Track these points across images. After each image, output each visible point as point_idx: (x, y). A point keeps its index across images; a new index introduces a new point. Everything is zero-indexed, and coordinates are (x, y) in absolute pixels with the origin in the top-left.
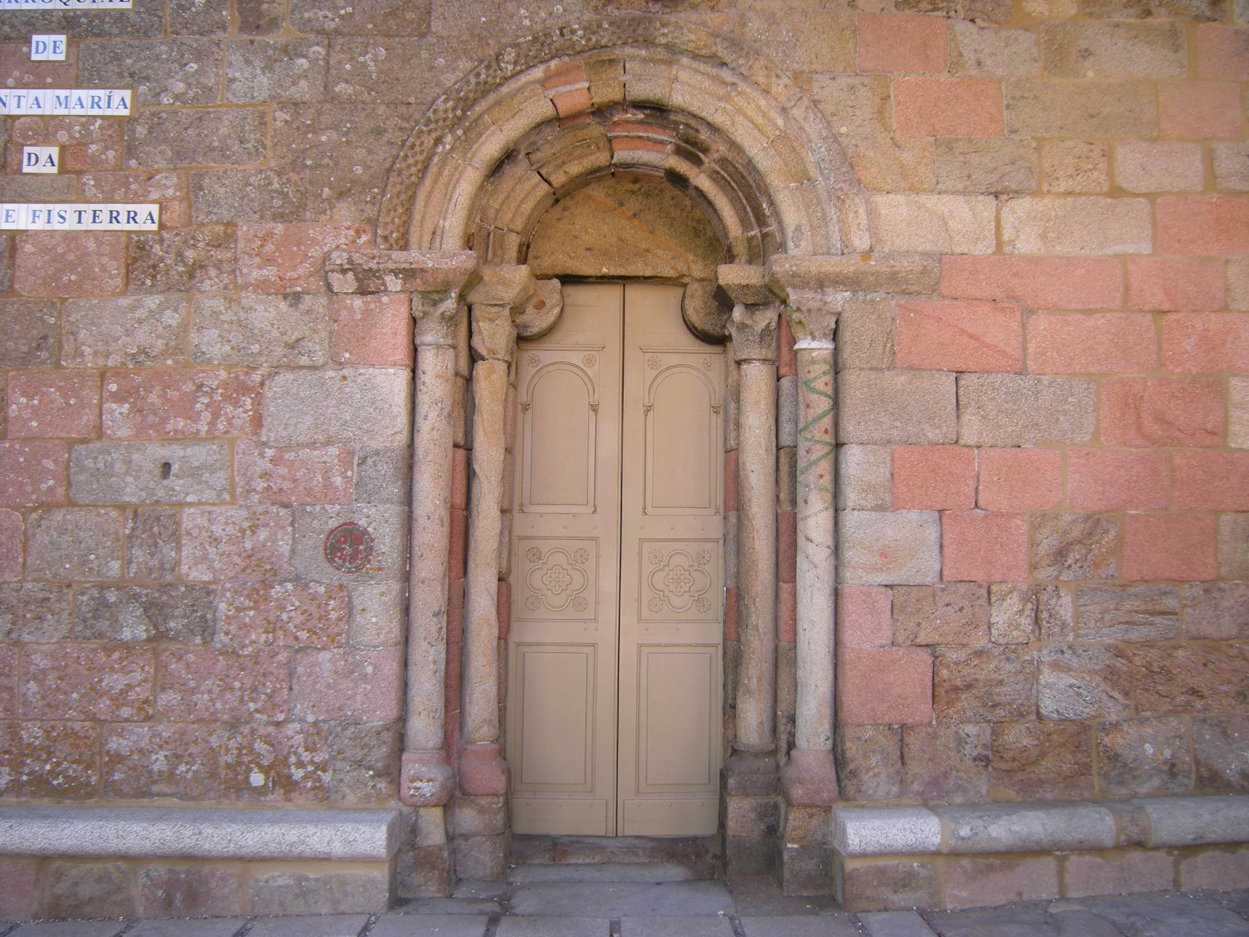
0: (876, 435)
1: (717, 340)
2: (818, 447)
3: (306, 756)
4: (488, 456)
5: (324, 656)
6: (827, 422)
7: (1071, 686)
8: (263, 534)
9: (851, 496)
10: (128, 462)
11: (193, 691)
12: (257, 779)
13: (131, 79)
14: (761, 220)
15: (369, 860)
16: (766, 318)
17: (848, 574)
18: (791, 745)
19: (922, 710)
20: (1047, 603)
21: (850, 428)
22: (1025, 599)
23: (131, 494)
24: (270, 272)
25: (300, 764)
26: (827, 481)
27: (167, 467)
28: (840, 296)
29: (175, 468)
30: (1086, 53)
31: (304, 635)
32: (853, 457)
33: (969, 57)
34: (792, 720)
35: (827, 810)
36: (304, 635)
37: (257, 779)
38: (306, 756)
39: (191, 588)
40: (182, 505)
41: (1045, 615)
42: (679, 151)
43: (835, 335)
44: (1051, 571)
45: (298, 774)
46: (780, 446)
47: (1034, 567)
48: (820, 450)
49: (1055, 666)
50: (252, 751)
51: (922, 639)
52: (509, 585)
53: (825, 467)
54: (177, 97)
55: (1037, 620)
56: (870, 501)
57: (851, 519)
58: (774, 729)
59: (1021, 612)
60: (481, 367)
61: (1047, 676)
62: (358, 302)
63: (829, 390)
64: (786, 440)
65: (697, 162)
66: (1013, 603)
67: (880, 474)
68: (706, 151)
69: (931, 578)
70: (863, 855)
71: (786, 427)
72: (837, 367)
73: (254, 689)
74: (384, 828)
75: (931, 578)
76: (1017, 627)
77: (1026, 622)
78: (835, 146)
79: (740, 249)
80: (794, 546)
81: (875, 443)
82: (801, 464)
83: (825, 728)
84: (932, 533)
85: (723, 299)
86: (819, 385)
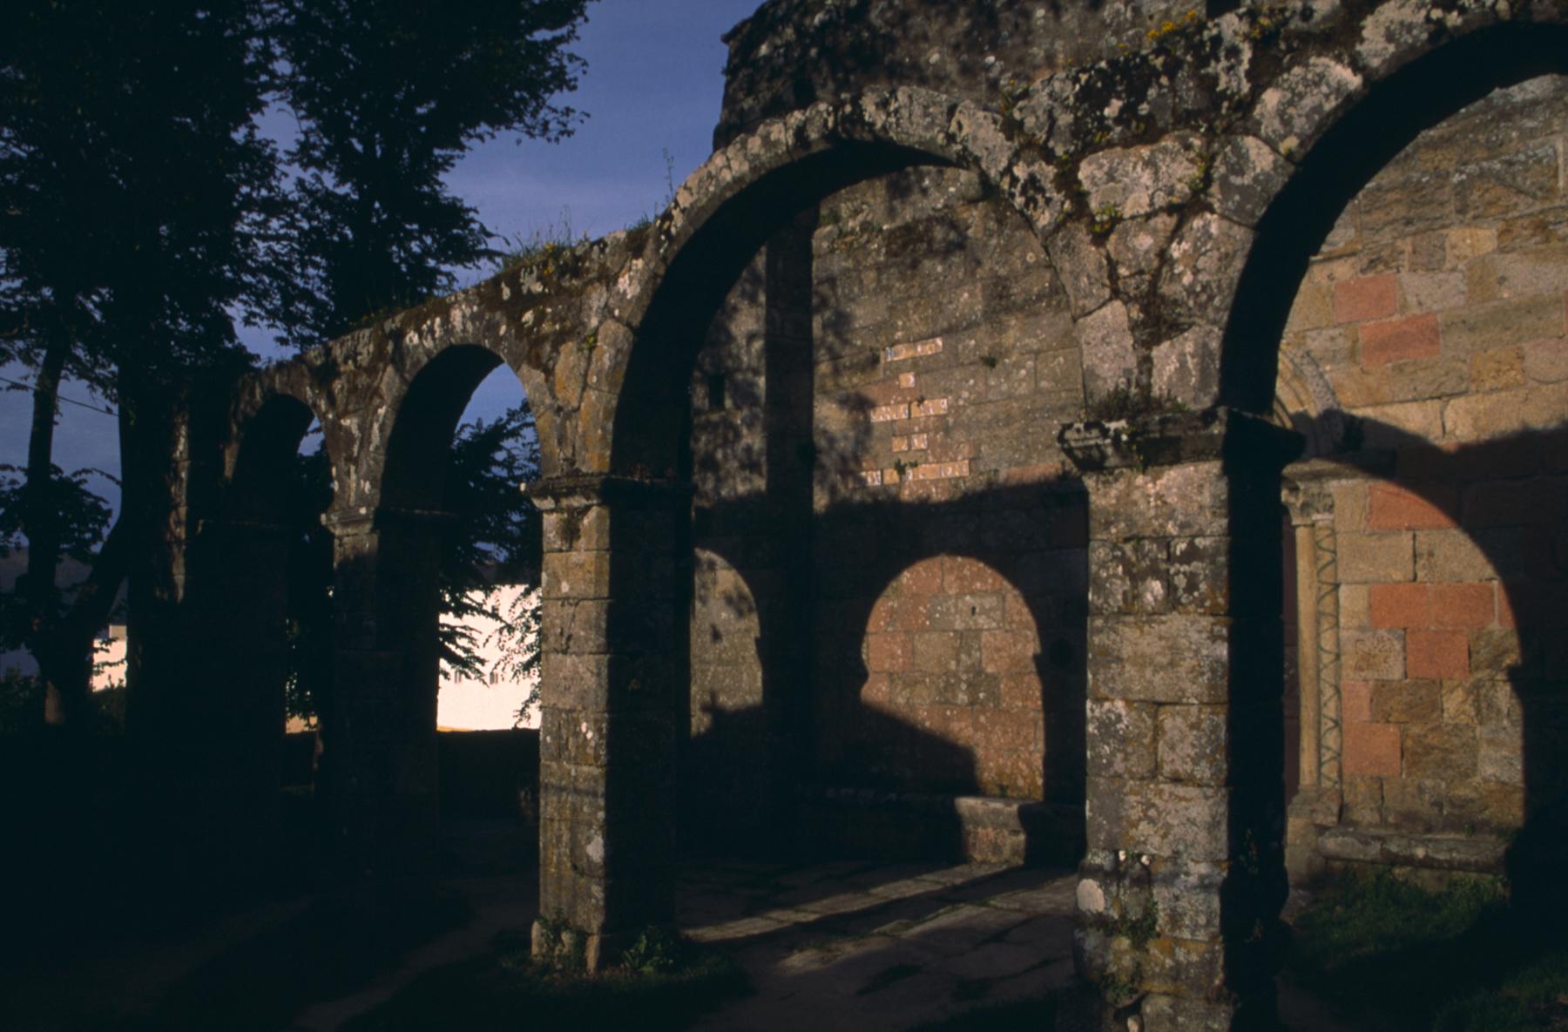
0: (1357, 578)
2: (1325, 586)
7: (1505, 757)
8: (1019, 646)
10: (956, 606)
11: (991, 732)
13: (946, 392)
20: (1486, 696)
22: (1468, 692)
23: (959, 625)
27: (974, 609)
28: (1098, 861)
29: (978, 610)
33: (1412, 300)
39: (987, 675)
40: (981, 630)
41: (1484, 705)
49: (1491, 742)
50: (1018, 767)
54: (965, 400)
56: (1355, 622)
59: (1464, 702)
61: (1484, 751)
66: (1459, 695)
67: (1361, 605)
73: (1018, 733)
74: (1291, 923)
76: (1463, 712)
78: (1321, 382)
81: (1356, 583)
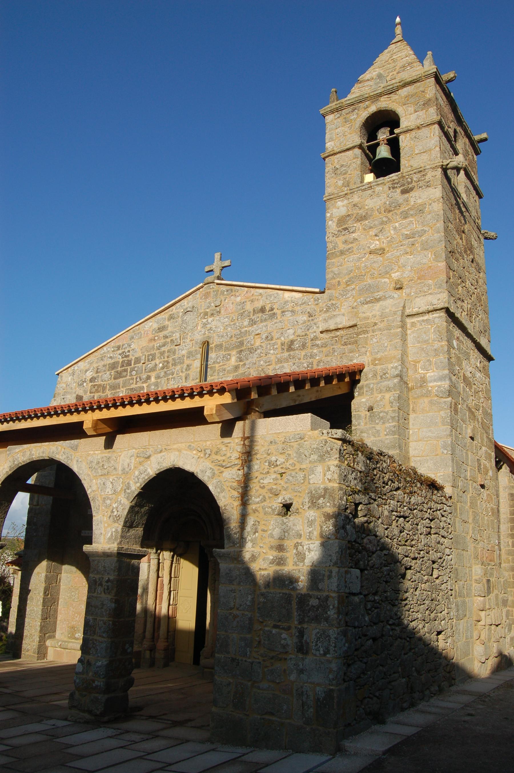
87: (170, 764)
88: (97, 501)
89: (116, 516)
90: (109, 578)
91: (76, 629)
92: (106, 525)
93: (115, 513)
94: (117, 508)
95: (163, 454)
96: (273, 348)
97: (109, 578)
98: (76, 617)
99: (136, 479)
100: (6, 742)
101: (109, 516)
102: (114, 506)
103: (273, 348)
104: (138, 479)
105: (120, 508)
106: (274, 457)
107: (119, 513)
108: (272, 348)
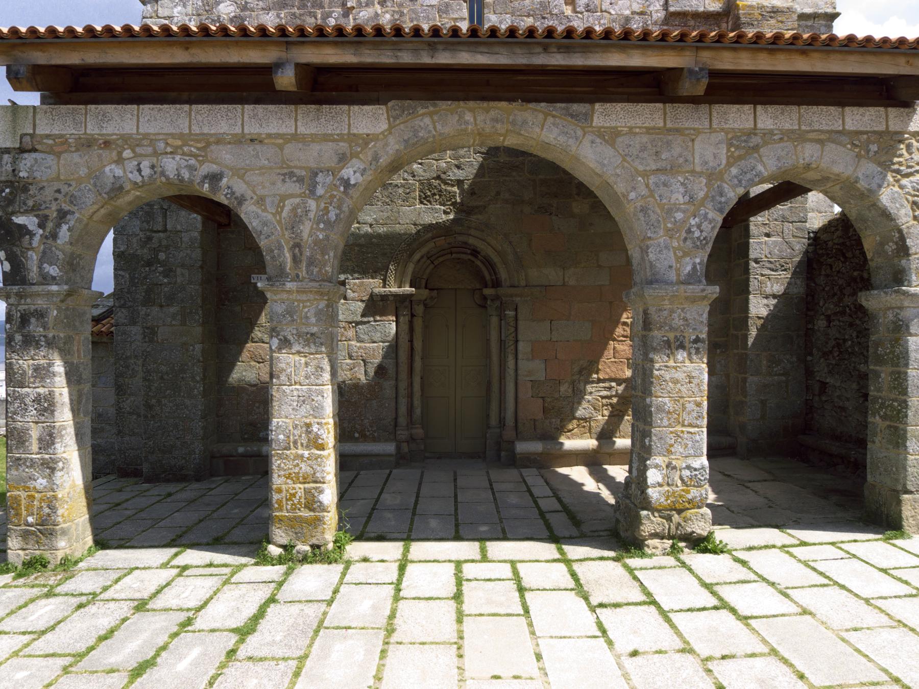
1: (484, 307)
3: (370, 429)
4: (418, 345)
5: (374, 402)
6: (514, 335)
9: (520, 356)
12: (357, 435)
14: (495, 274)
15: (390, 455)
16: (498, 303)
17: (519, 378)
18: (504, 425)
19: (540, 416)
21: (520, 337)
24: (356, 295)
25: (368, 431)
26: (513, 351)
30: (591, 224)
31: (369, 396)
32: (521, 345)
34: (504, 418)
35: (513, 442)
36: (369, 396)
37: (357, 435)
38: (370, 429)
42: (471, 254)
43: (516, 310)
44: (578, 376)
45: (368, 433)
46: (452, 604)
47: (573, 375)
48: (511, 343)
51: (540, 395)
52: (807, 678)
53: (513, 347)
55: (573, 390)
57: (520, 362)
58: (500, 421)
60: (415, 319)
62: (381, 303)
63: (514, 325)
64: (503, 338)
65: (476, 257)
66: (566, 385)
68: (479, 253)
69: (543, 379)
70: (521, 454)
71: (503, 335)
72: (516, 319)
75: (543, 379)
77: (570, 390)
79: (489, 283)
80: (505, 369)
82: (507, 346)
83: (513, 420)
84: (543, 366)
85: (485, 298)
86: (512, 324)
87: (158, 502)
88: (345, 208)
89: (698, 238)
90: (697, 336)
91: (259, 425)
92: (680, 254)
93: (697, 234)
94: (699, 226)
95: (785, 144)
96: (599, 23)
97: (697, 336)
98: (258, 408)
99: (736, 181)
100: (904, 589)
101: (682, 238)
102: (693, 223)
103: (599, 23)
104: (740, 181)
105: (706, 226)
106: (321, 180)
107: (704, 234)
108: (597, 22)
